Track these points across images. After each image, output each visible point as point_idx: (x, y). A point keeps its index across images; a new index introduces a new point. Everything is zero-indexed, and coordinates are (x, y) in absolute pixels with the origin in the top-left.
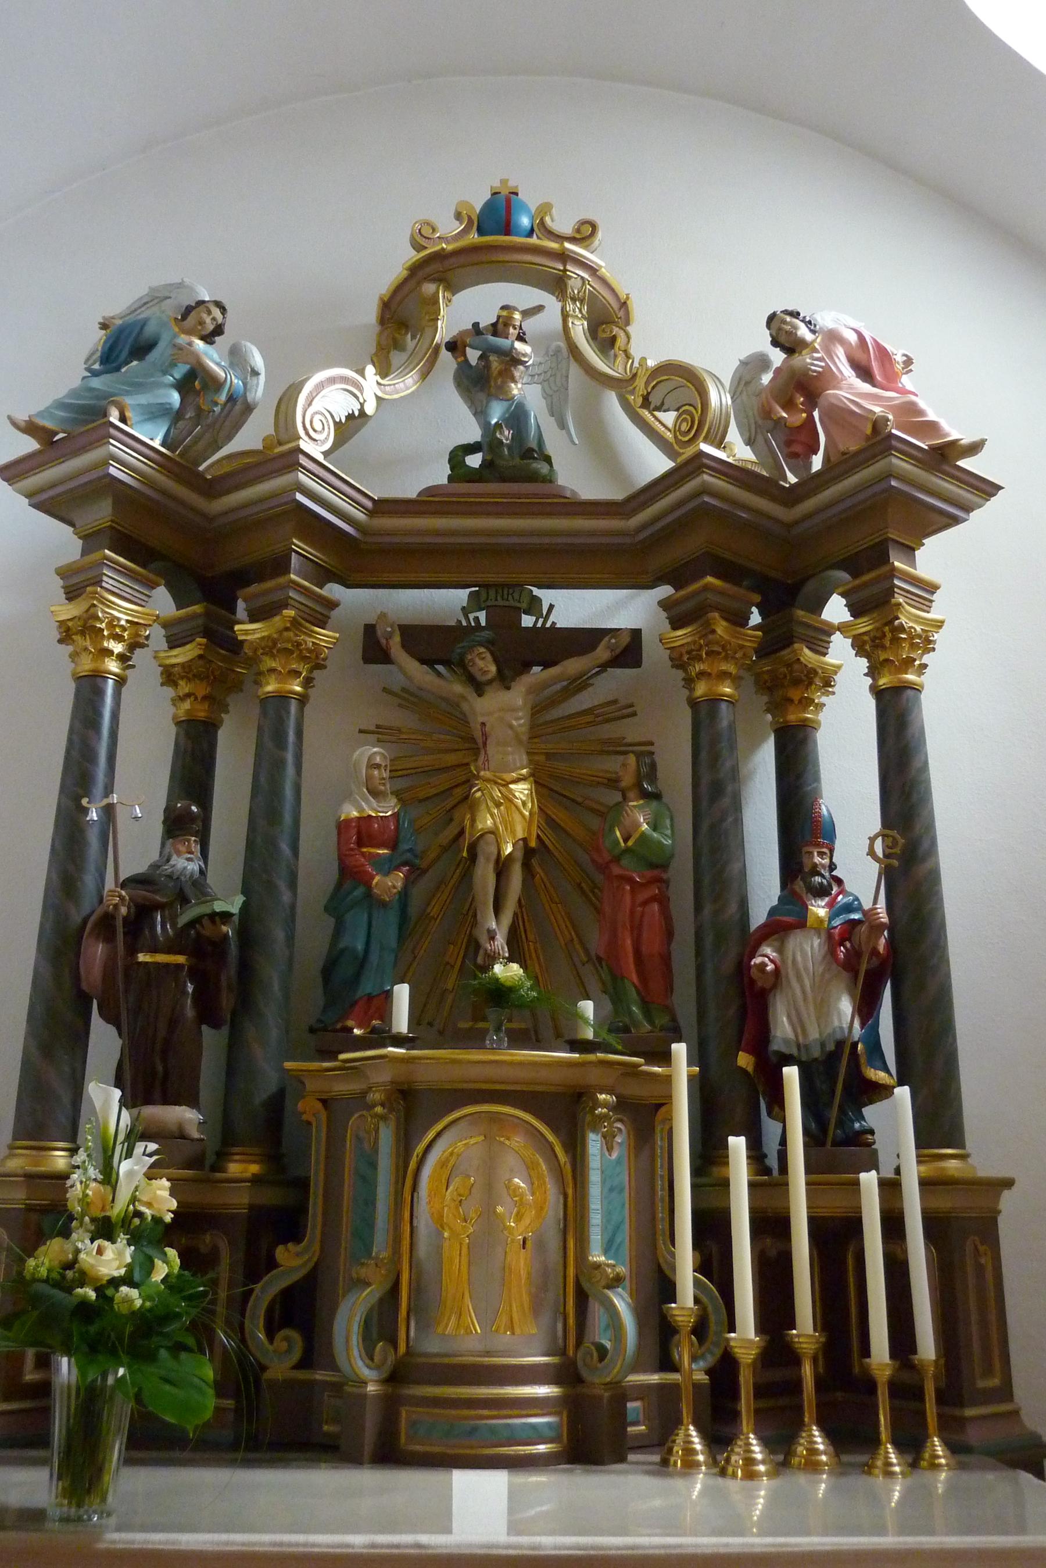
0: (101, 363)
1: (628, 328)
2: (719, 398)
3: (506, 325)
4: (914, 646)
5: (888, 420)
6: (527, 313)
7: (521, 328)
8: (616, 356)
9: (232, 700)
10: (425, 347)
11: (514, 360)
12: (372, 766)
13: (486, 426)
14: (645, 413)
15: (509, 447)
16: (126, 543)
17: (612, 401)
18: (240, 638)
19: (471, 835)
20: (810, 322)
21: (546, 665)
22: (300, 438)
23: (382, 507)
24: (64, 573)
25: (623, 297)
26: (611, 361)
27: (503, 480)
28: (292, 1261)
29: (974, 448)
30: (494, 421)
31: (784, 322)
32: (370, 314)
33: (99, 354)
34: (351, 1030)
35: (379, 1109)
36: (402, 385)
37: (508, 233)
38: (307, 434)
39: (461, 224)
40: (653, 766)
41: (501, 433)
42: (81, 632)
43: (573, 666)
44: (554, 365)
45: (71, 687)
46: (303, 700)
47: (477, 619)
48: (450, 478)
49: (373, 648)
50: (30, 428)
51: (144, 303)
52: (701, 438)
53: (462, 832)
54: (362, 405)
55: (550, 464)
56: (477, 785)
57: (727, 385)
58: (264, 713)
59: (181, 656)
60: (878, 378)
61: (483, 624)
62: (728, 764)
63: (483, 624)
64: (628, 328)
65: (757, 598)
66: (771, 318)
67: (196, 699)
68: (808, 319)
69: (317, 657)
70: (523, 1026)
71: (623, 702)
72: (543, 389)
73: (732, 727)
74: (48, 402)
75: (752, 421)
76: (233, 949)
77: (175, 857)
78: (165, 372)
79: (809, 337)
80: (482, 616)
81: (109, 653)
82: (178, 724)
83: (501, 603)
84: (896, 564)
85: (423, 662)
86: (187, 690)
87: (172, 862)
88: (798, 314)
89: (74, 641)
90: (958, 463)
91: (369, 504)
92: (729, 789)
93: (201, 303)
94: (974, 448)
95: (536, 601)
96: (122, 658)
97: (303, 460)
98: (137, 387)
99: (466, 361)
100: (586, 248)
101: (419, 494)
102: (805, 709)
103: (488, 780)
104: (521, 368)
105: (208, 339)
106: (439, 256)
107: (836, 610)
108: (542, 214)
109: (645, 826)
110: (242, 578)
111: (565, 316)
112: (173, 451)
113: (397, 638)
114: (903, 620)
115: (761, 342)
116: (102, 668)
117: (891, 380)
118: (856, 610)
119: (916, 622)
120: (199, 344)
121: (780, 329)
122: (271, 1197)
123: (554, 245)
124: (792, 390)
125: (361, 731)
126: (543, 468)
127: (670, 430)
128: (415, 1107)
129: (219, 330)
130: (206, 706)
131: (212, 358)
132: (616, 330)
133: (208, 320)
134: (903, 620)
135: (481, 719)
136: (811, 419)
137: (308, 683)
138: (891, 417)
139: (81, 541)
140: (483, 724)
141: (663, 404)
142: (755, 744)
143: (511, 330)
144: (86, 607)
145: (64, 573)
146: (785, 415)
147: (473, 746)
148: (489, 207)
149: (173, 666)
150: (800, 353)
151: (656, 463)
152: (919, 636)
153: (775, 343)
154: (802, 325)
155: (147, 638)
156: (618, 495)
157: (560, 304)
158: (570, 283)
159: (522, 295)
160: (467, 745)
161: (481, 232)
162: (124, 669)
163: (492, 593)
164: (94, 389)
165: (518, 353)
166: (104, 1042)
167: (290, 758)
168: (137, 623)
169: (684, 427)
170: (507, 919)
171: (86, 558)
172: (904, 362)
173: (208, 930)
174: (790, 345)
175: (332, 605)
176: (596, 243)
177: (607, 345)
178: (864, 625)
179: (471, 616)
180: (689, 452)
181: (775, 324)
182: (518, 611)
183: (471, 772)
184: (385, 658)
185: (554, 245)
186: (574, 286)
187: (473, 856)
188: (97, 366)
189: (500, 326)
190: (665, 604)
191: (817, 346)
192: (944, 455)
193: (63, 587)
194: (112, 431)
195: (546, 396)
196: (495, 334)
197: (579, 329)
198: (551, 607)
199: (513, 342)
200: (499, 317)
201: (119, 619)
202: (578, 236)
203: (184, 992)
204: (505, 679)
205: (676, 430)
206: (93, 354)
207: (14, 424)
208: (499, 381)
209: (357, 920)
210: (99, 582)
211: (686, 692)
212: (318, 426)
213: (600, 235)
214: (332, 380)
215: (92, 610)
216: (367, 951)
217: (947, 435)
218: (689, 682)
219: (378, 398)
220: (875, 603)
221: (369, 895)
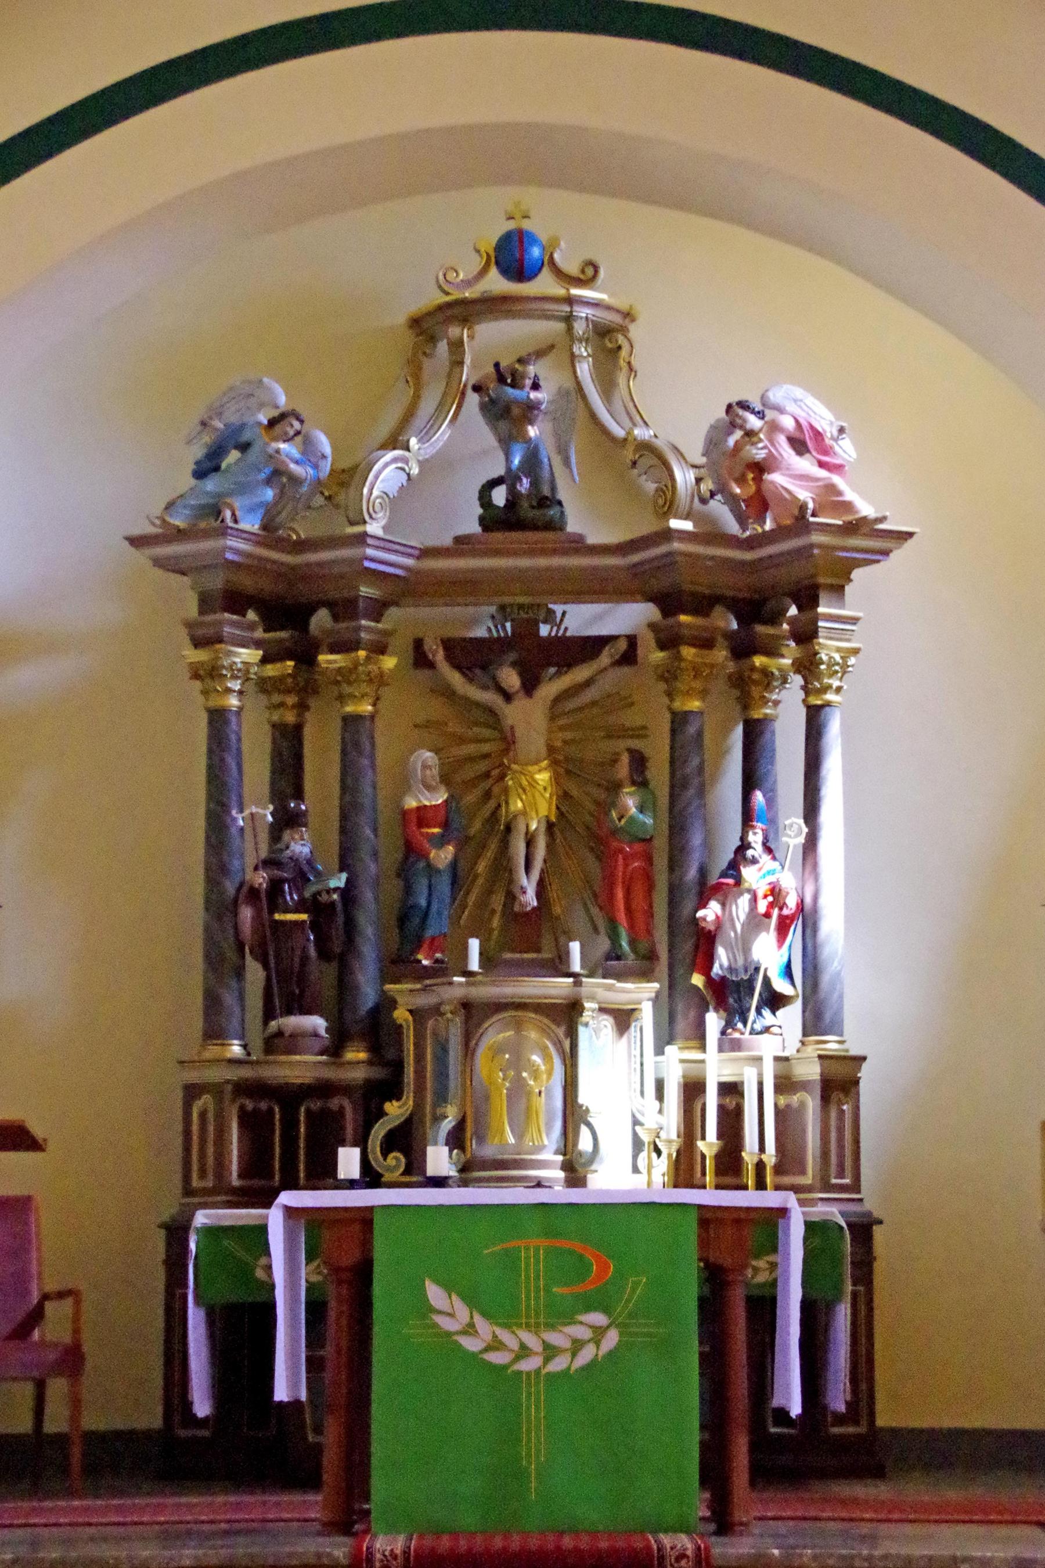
2: (684, 477)
9: (313, 702)
12: (425, 767)
19: (507, 816)
23: (426, 553)
28: (395, 1111)
29: (882, 519)
32: (401, 319)
34: (420, 961)
35: (449, 1015)
43: (580, 674)
46: (372, 717)
49: (421, 659)
53: (499, 806)
59: (271, 670)
62: (695, 762)
70: (550, 956)
76: (339, 907)
77: (292, 844)
81: (229, 691)
82: (274, 726)
87: (292, 848)
92: (696, 782)
95: (551, 613)
96: (241, 693)
100: (592, 289)
108: (551, 249)
109: (634, 810)
122: (377, 1073)
128: (474, 1014)
142: (736, 724)
144: (213, 656)
146: (738, 491)
152: (838, 664)
166: (255, 973)
170: (535, 875)
173: (324, 898)
175: (386, 633)
182: (536, 624)
184: (431, 665)
187: (508, 829)
191: (762, 436)
194: (229, 531)
198: (564, 614)
202: (582, 277)
203: (308, 940)
204: (530, 686)
209: (421, 886)
216: (429, 904)
221: (429, 865)
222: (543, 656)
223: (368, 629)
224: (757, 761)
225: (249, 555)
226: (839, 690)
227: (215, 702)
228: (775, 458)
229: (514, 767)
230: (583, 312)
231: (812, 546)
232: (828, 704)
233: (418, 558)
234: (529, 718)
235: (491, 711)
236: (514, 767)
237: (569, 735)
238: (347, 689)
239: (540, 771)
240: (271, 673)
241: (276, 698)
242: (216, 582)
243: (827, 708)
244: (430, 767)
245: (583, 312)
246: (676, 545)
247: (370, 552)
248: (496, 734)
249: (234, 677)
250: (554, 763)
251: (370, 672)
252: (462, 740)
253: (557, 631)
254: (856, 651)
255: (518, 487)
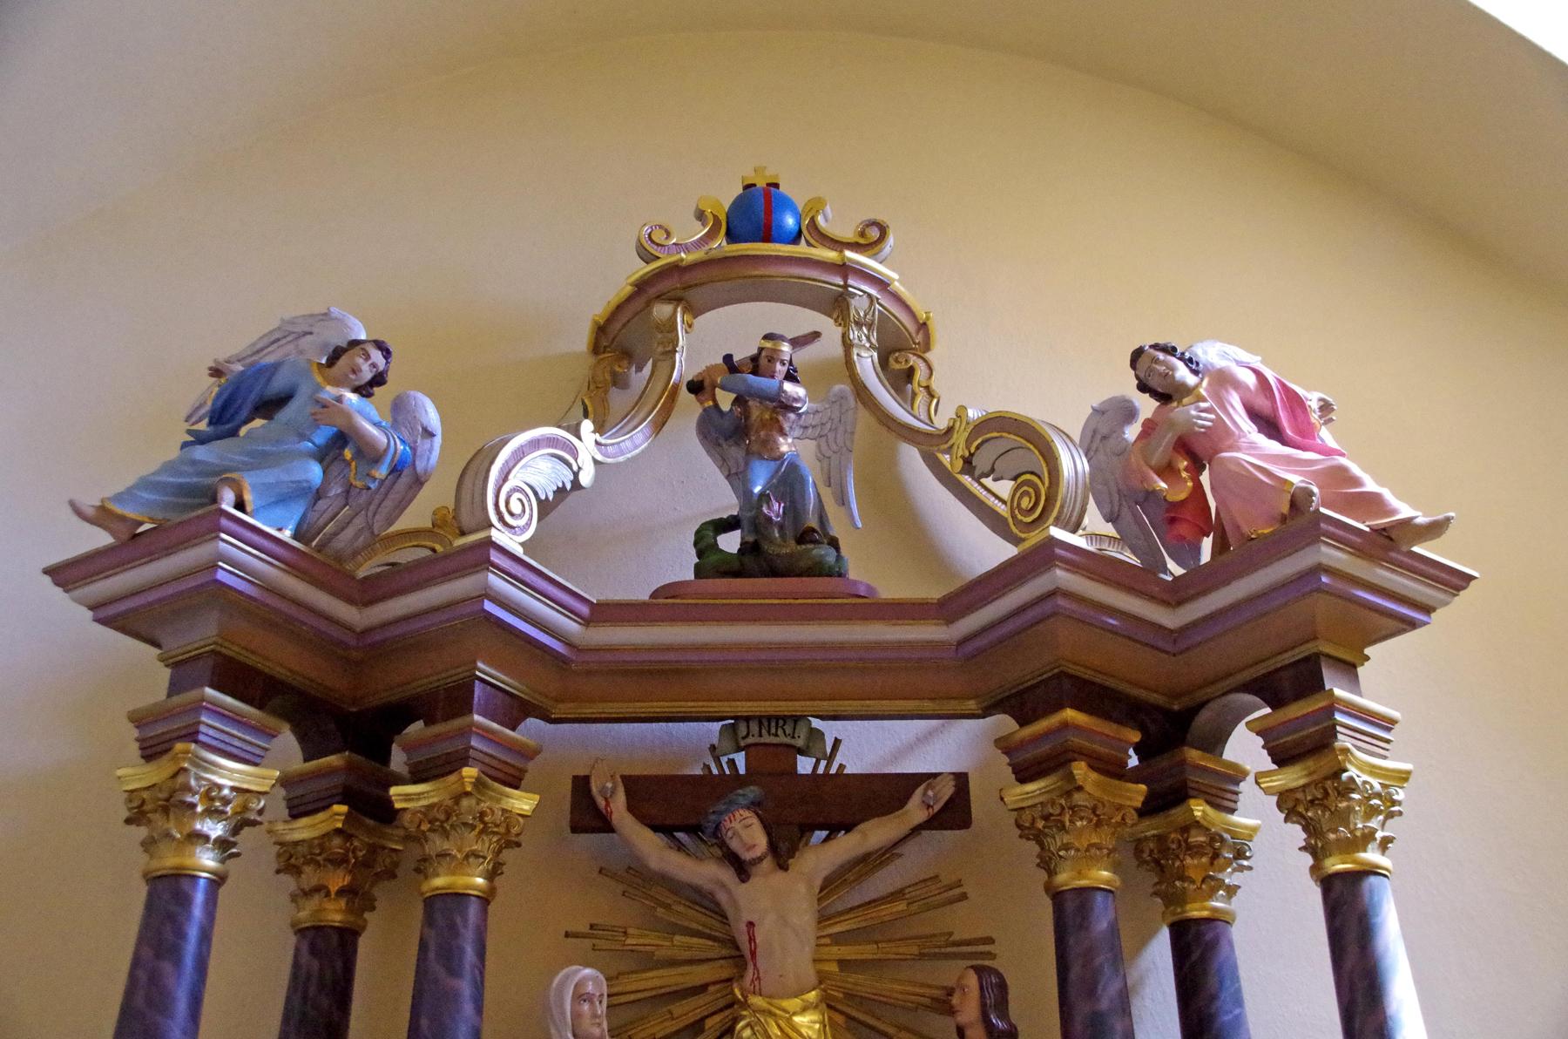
0: (210, 423)
1: (927, 355)
2: (1072, 464)
3: (771, 360)
4: (1372, 812)
5: (1311, 494)
6: (797, 343)
7: (791, 363)
8: (914, 395)
9: (380, 892)
10: (659, 388)
11: (785, 406)
12: (580, 997)
13: (744, 494)
14: (966, 480)
15: (781, 527)
16: (237, 677)
17: (911, 458)
18: (398, 806)
20: (1190, 360)
21: (837, 827)
22: (491, 525)
23: (602, 613)
24: (139, 720)
25: (922, 316)
26: (909, 401)
27: (774, 572)
29: (1435, 529)
30: (757, 489)
31: (1157, 361)
32: (581, 341)
33: (208, 407)
36: (628, 444)
37: (767, 239)
38: (501, 519)
39: (704, 225)
40: (1002, 987)
41: (769, 508)
42: (158, 810)
43: (875, 833)
44: (836, 415)
45: (141, 892)
46: (485, 900)
47: (732, 763)
48: (699, 571)
49: (587, 814)
50: (102, 517)
51: (273, 340)
52: (1051, 520)
54: (576, 475)
55: (837, 549)
56: (743, 1018)
57: (1077, 439)
58: (429, 920)
59: (305, 830)
60: (1289, 432)
61: (742, 771)
62: (1114, 988)
63: (742, 771)
64: (927, 355)
65: (1136, 737)
66: (1137, 355)
67: (328, 894)
68: (1187, 355)
69: (508, 831)
71: (946, 879)
72: (819, 446)
73: (1114, 930)
74: (130, 480)
75: (1114, 489)
78: (303, 437)
79: (1191, 380)
80: (740, 759)
82: (301, 932)
83: (767, 739)
84: (1338, 692)
85: (655, 828)
86: (314, 882)
88: (1174, 349)
89: (150, 821)
90: (1416, 549)
91: (585, 610)
93: (355, 343)
94: (1435, 529)
95: (817, 735)
96: (223, 844)
97: (495, 557)
98: (261, 460)
99: (716, 406)
100: (872, 257)
101: (654, 595)
102: (1212, 894)
103: (763, 1011)
104: (792, 416)
105: (364, 390)
106: (675, 269)
107: (1244, 748)
110: (398, 715)
111: (847, 345)
112: (307, 543)
113: (620, 799)
114: (1352, 772)
115: (1125, 385)
116: (188, 862)
117: (1304, 437)
118: (1282, 757)
119: (1371, 774)
120: (352, 398)
121: (1150, 370)
123: (830, 255)
124: (1165, 451)
125: (567, 935)
126: (826, 553)
127: (1004, 502)
129: (379, 379)
130: (342, 903)
131: (367, 418)
132: (913, 360)
133: (365, 367)
134: (1352, 772)
135: (746, 917)
136: (1198, 486)
137: (491, 875)
138: (1316, 490)
139: (167, 672)
140: (751, 924)
141: (993, 470)
143: (779, 367)
145: (139, 720)
146: (1163, 485)
147: (734, 953)
148: (741, 205)
149: (296, 843)
150: (1180, 402)
151: (986, 551)
152: (1378, 796)
153: (1143, 387)
154: (1180, 365)
155: (260, 812)
156: (935, 593)
157: (840, 329)
158: (853, 302)
159: (795, 319)
160: (725, 952)
161: (732, 237)
162: (222, 861)
163: (754, 727)
164: (200, 462)
165: (789, 397)
167: (465, 987)
168: (248, 791)
169: (1025, 503)
171: (176, 699)
172: (1321, 408)
174: (1167, 394)
175: (528, 753)
176: (887, 249)
177: (901, 380)
178: (1293, 777)
179: (724, 760)
180: (1034, 538)
181: (1143, 362)
183: (732, 993)
185: (830, 255)
186: (859, 305)
188: (203, 426)
189: (763, 361)
190: (1005, 746)
191: (1202, 391)
192: (1390, 541)
193: (137, 740)
194: (224, 522)
195: (821, 457)
196: (755, 372)
197: (866, 363)
198: (837, 742)
199: (781, 383)
200: (761, 350)
201: (220, 787)
202: (862, 241)
204: (782, 852)
205: (1014, 504)
206: (198, 408)
207: (79, 513)
208: (762, 433)
210: (192, 735)
211: (1044, 875)
212: (516, 507)
213: (891, 240)
214: (535, 444)
215: (180, 779)
217: (1393, 512)
218: (1048, 864)
219: (596, 462)
220: (1306, 746)
222: (815, 808)
223: (486, 735)
224: (1214, 998)
225: (270, 589)
226: (1385, 844)
227: (169, 860)
228: (1228, 433)
229: (756, 1001)
230: (858, 285)
231: (1320, 569)
232: (1372, 871)
233: (587, 622)
234: (782, 909)
235: (704, 901)
236: (756, 1001)
237: (847, 952)
238: (437, 844)
239: (804, 1010)
240: (297, 836)
241: (310, 877)
242: (203, 633)
243: (1373, 879)
244: (588, 998)
245: (858, 285)
246: (1061, 576)
247: (496, 582)
248: (716, 950)
249: (211, 813)
250: (828, 1004)
251: (482, 814)
252: (649, 962)
253: (828, 766)
254: (1403, 777)
255: (765, 510)
